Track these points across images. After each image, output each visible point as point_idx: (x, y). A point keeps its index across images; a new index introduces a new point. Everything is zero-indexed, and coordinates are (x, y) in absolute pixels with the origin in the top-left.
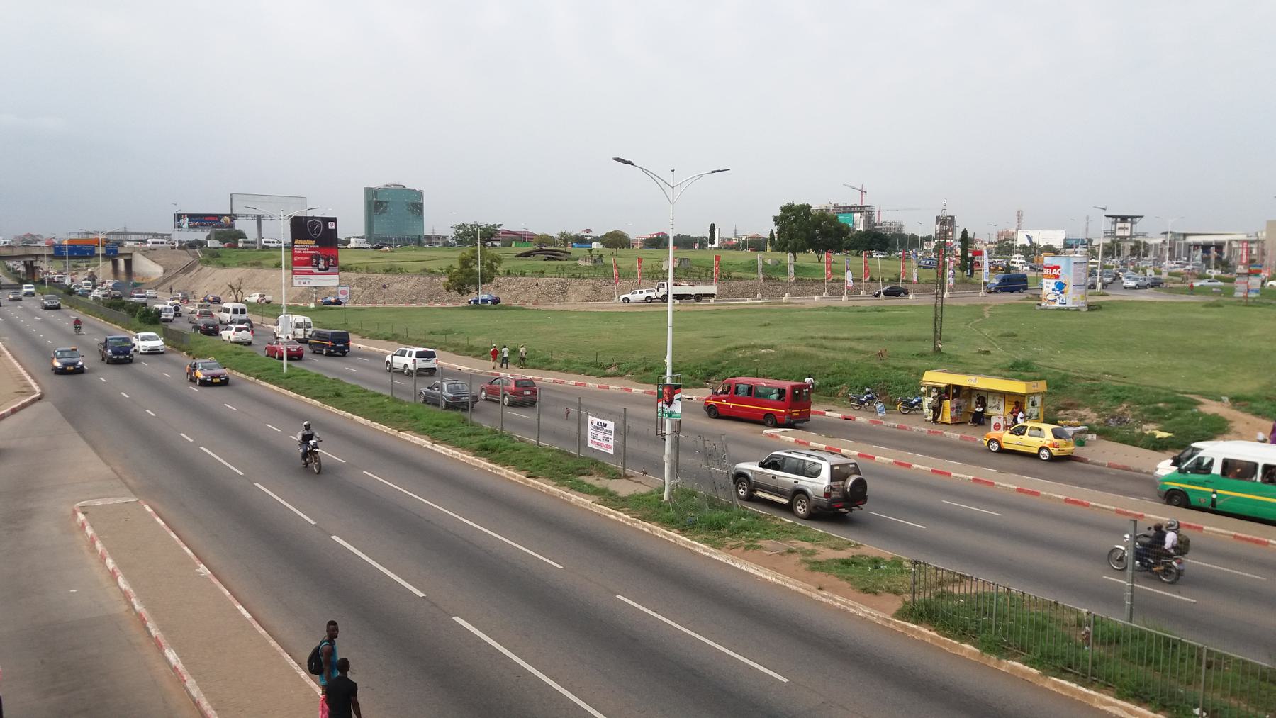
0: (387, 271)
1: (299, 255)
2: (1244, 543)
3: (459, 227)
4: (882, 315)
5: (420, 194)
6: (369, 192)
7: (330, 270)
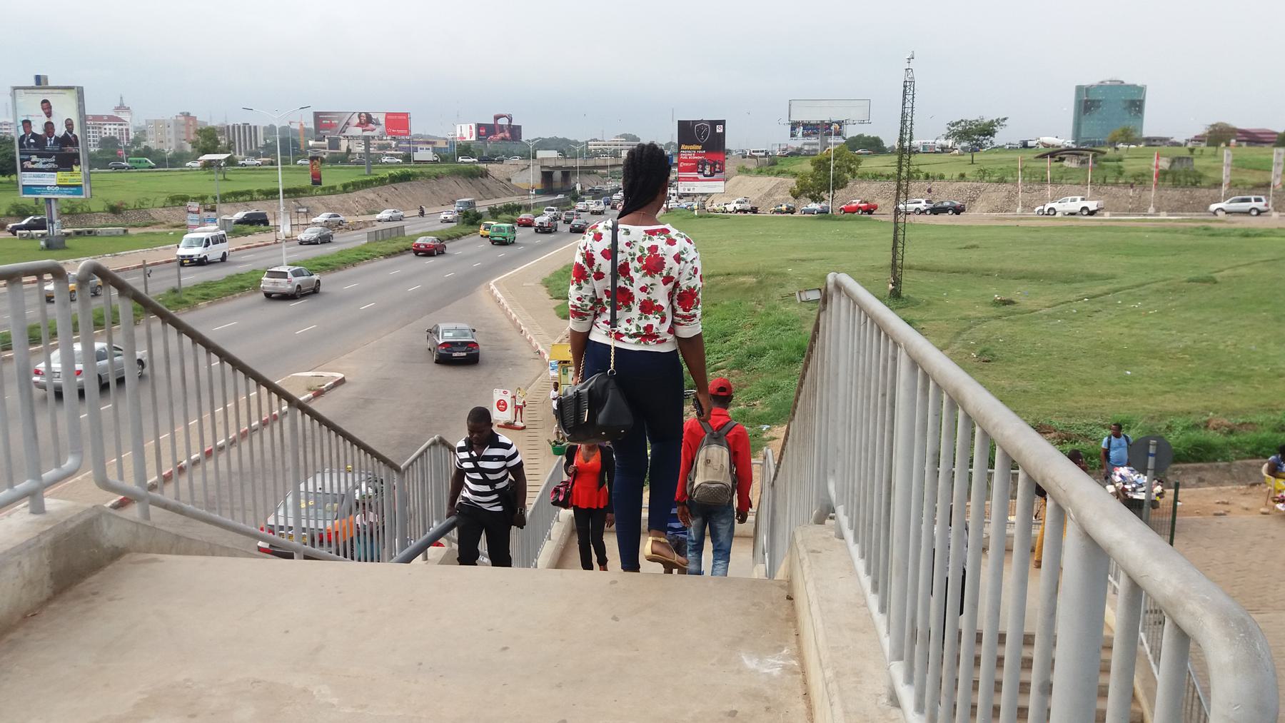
1: (685, 161)
2: (231, 534)
4: (1213, 241)
5: (1141, 90)
6: (1079, 89)
7: (716, 176)
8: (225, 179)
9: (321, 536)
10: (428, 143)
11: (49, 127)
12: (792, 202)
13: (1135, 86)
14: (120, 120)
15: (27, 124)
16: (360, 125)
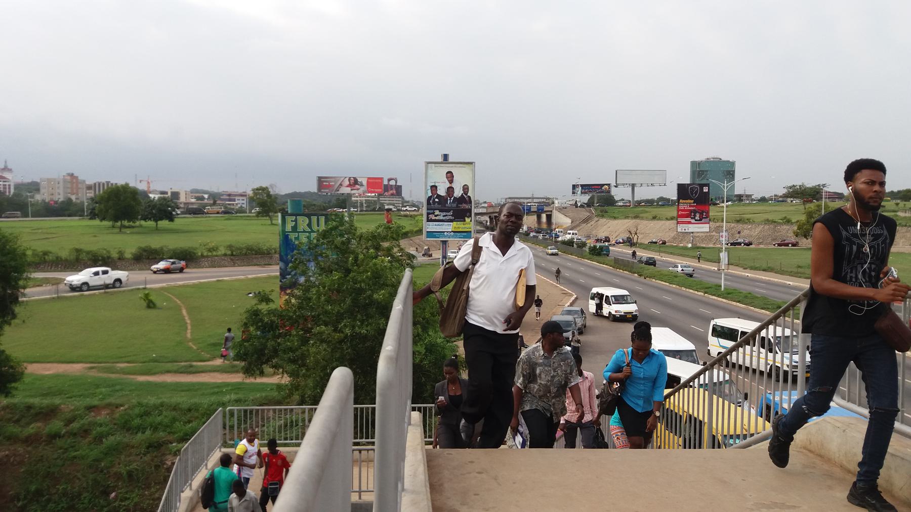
0: (738, 221)
3: (790, 188)
5: (733, 164)
6: (694, 164)
7: (703, 221)
8: (272, 224)
9: (785, 380)
10: (242, 195)
11: (450, 190)
12: (794, 240)
13: (728, 161)
14: (4, 178)
15: (434, 188)
16: (349, 185)
